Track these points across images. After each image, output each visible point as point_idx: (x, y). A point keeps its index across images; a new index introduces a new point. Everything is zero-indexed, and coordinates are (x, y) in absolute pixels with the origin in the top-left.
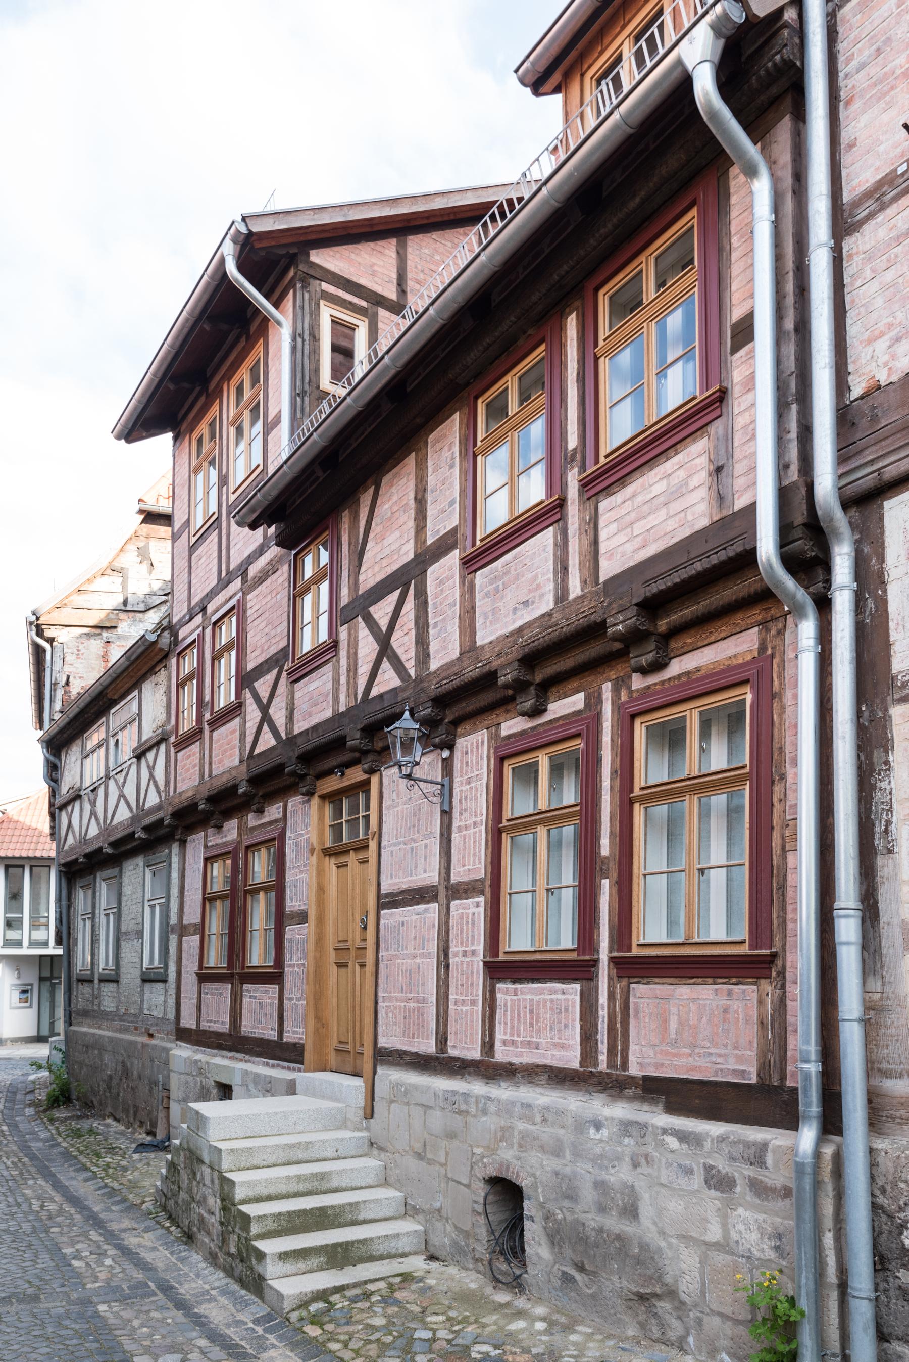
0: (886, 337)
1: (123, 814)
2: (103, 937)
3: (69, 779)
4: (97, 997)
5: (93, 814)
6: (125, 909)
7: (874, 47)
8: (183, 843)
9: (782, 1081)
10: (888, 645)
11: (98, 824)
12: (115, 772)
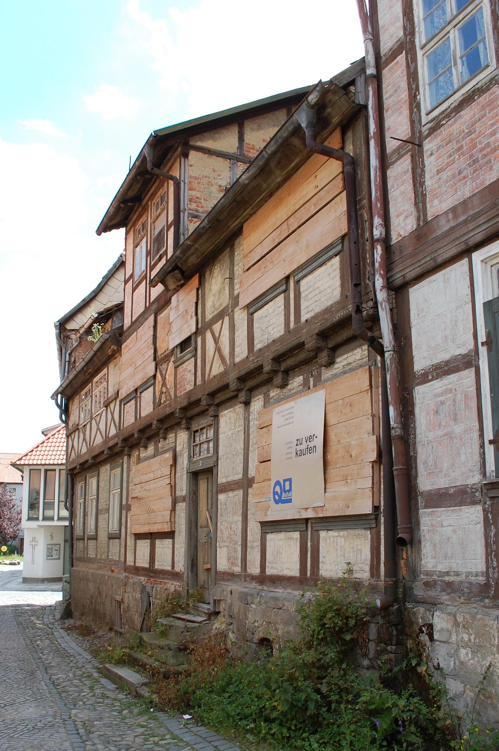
0: (403, 216)
1: (99, 440)
2: (89, 513)
3: (73, 419)
4: (86, 549)
5: (84, 439)
6: (100, 495)
7: (394, 89)
8: (129, 456)
9: (119, 559)
10: (412, 358)
11: (87, 446)
12: (95, 415)
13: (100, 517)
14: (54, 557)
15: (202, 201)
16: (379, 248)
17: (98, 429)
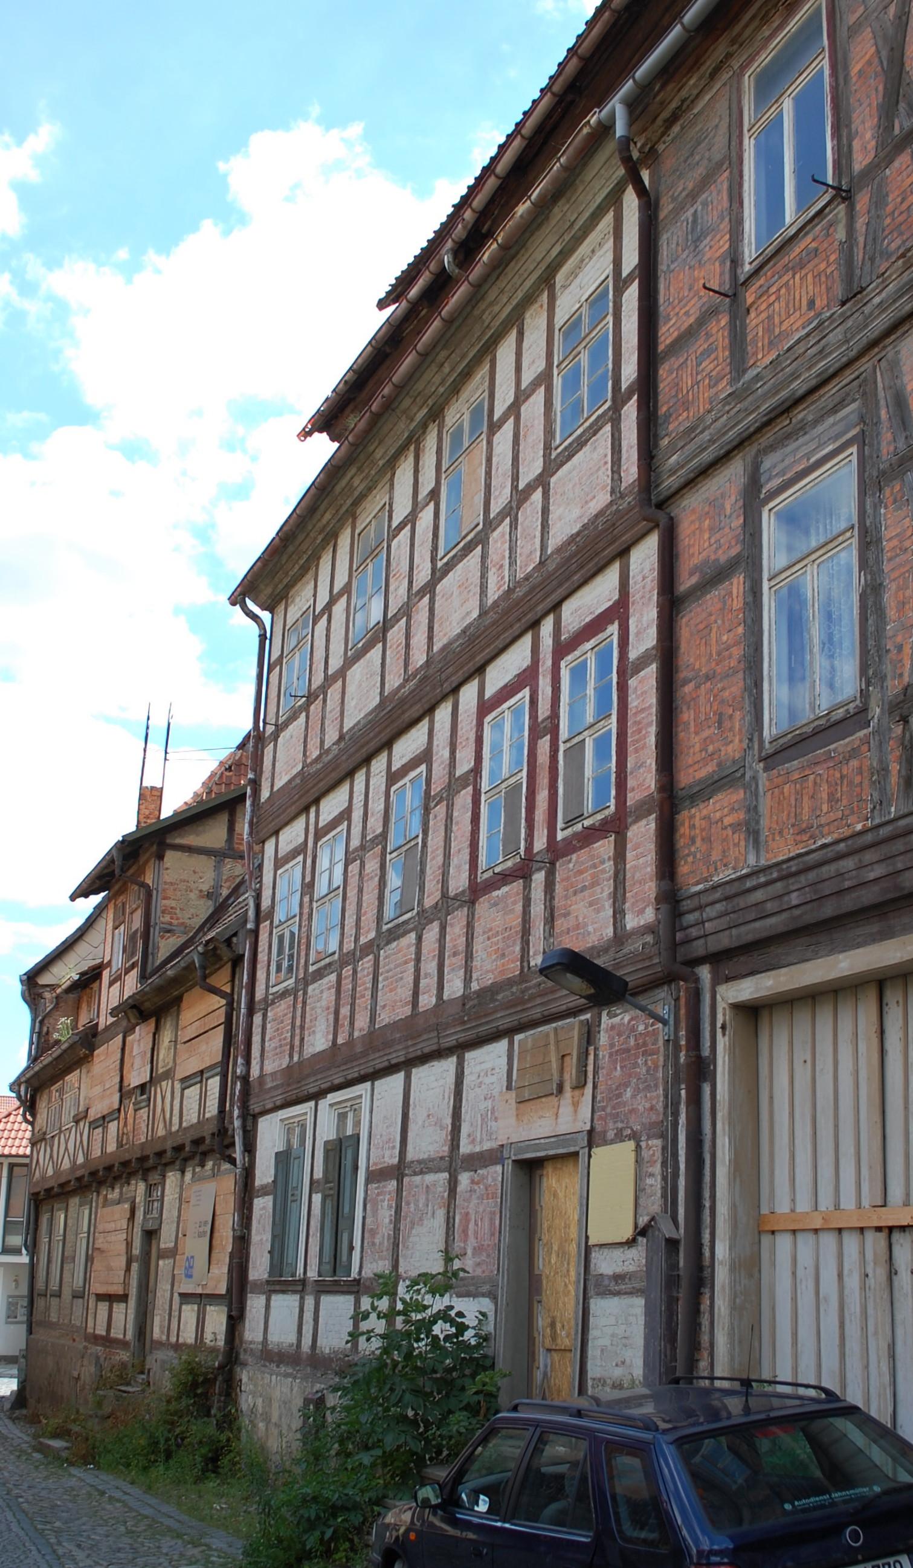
1: (66, 1164)
2: (54, 1259)
4: (48, 1308)
5: (51, 1157)
8: (98, 1193)
13: (66, 1267)
14: (19, 1318)
15: (178, 911)
16: (239, 1084)
17: (66, 1149)
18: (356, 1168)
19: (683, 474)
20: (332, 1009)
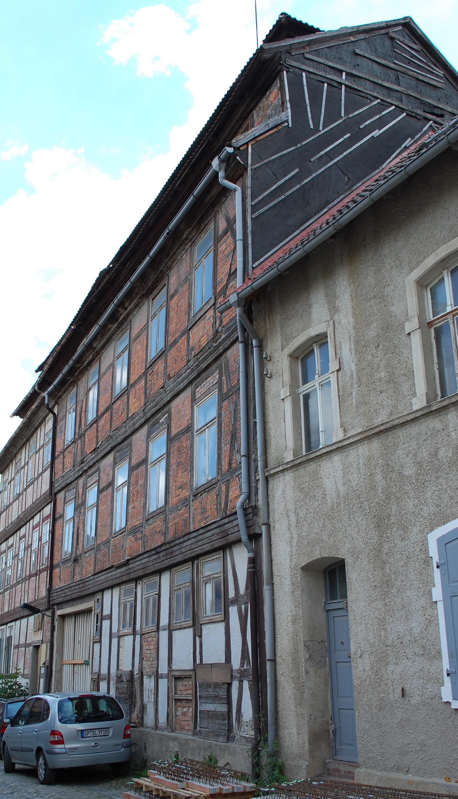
18: (11, 645)
19: (59, 488)
20: (383, 422)
